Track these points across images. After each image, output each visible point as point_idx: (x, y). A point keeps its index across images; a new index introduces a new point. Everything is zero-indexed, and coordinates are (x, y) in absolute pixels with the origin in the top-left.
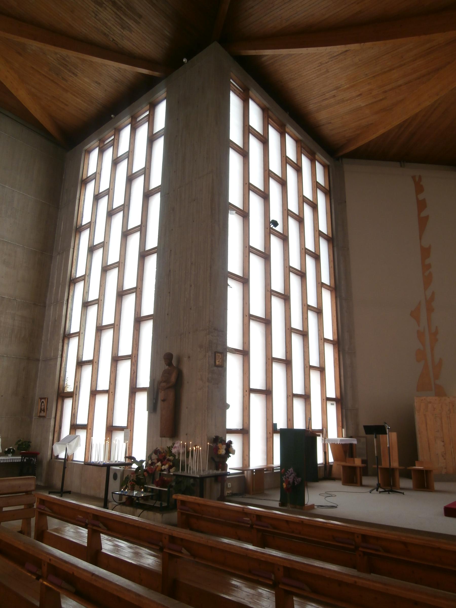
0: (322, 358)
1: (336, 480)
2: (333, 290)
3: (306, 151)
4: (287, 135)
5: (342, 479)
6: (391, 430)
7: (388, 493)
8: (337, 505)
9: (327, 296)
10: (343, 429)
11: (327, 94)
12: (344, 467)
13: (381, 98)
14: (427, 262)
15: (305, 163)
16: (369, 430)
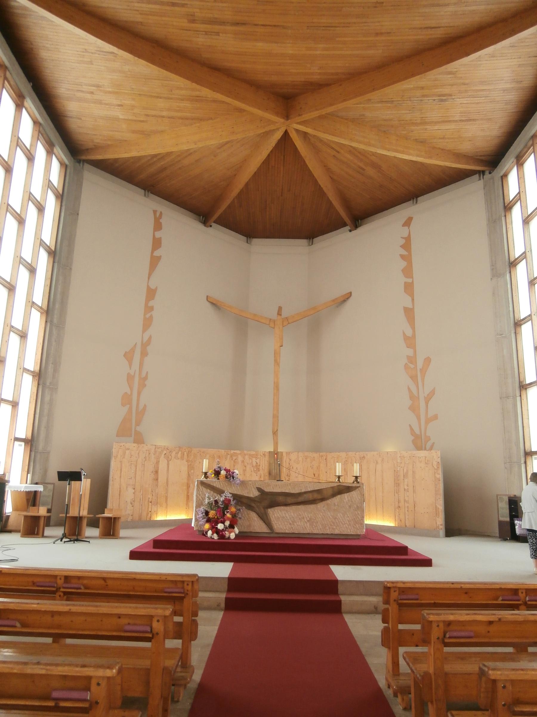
0: (18, 391)
1: (12, 533)
2: (44, 313)
3: (44, 138)
4: (54, 157)
5: (21, 531)
6: (86, 477)
7: (73, 542)
8: (17, 558)
9: (36, 318)
10: (29, 475)
11: (84, 87)
12: (26, 517)
13: (142, 119)
14: (151, 304)
15: (40, 152)
16: (64, 476)
